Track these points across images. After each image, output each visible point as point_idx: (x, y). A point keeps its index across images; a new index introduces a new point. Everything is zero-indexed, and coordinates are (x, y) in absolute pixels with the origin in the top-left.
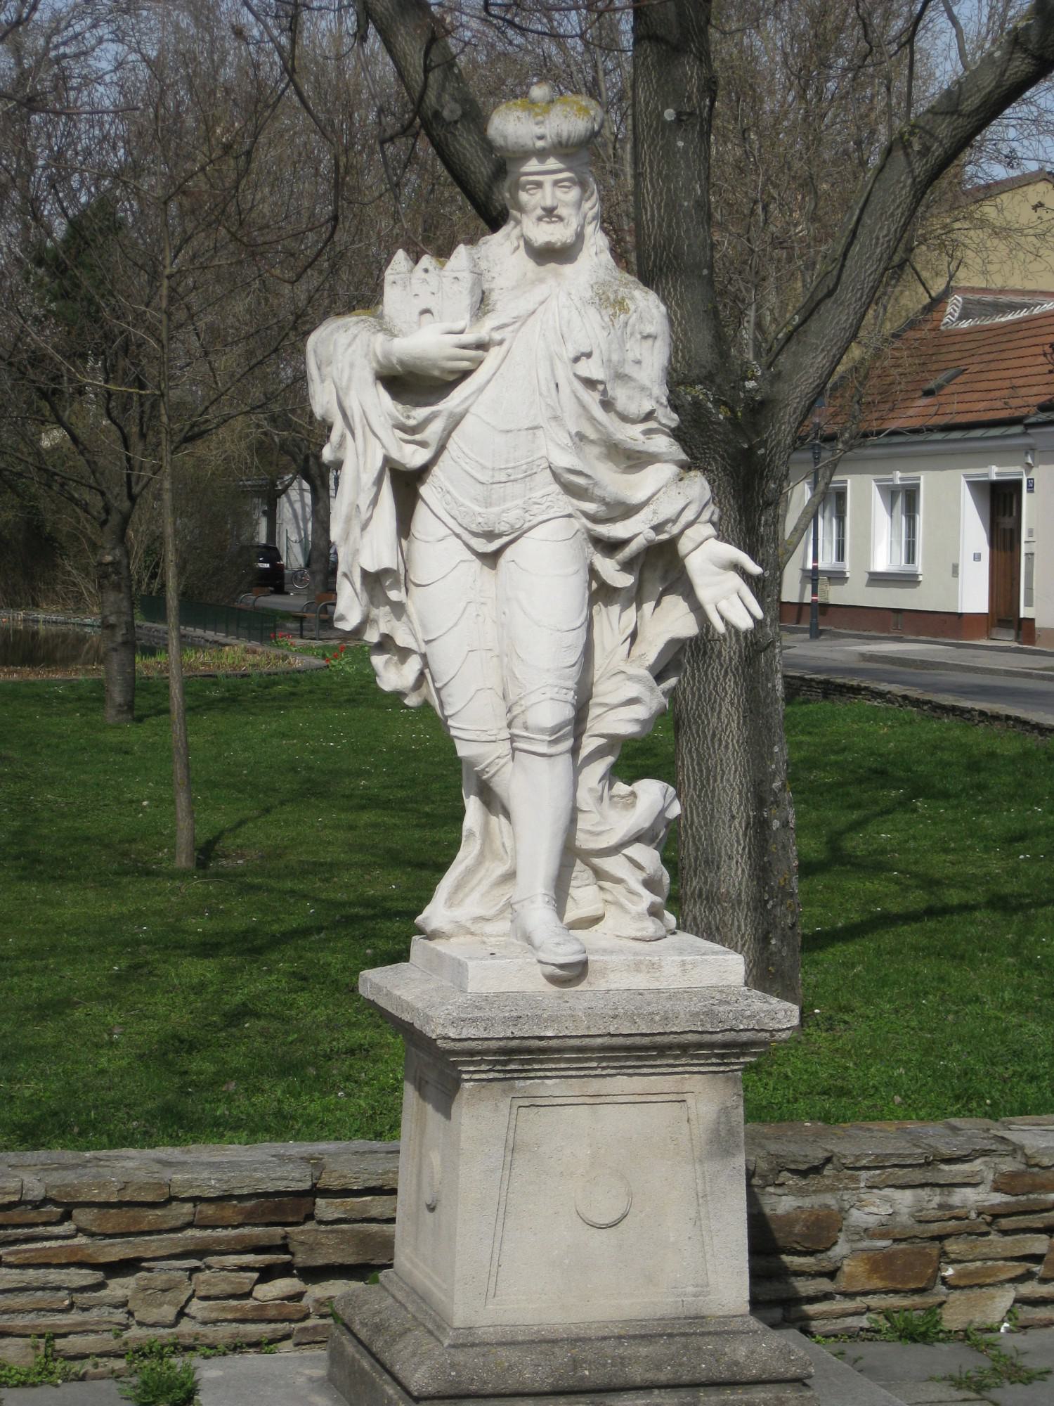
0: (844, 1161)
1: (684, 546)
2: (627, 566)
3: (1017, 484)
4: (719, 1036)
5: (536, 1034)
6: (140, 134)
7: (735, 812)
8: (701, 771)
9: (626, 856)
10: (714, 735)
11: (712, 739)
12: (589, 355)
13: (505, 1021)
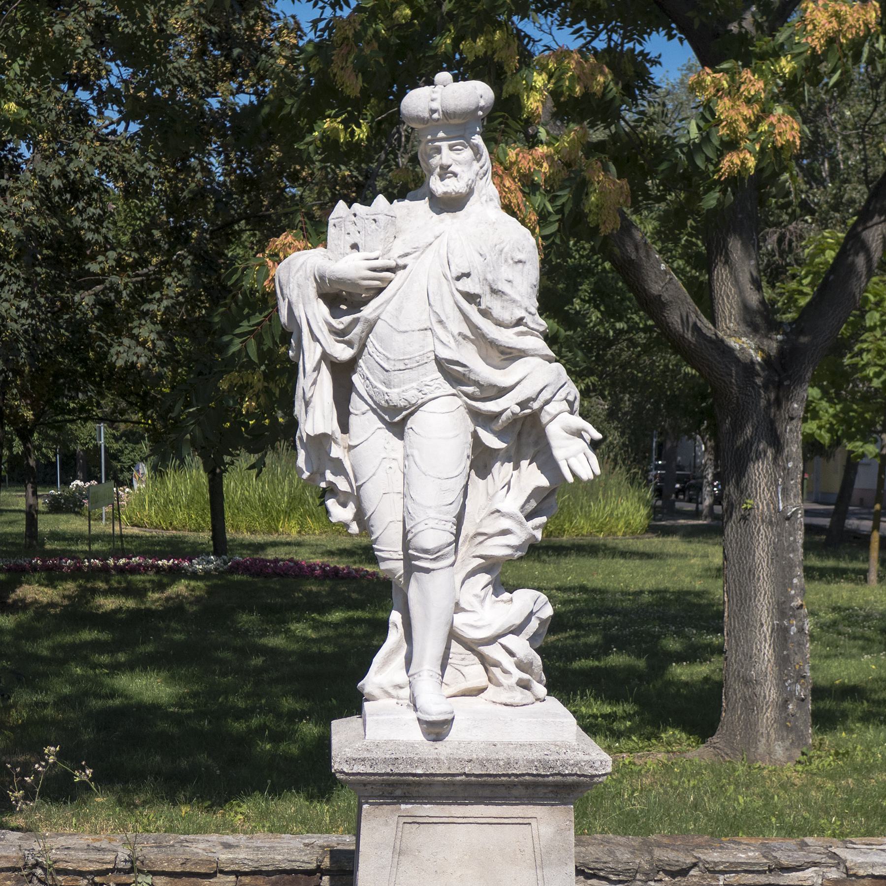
0: (707, 866)
1: (545, 418)
2: (500, 435)
4: (551, 778)
5: (410, 771)
7: (764, 622)
8: (741, 594)
9: (504, 647)
10: (750, 571)
11: (749, 573)
12: (468, 275)
13: (385, 761)
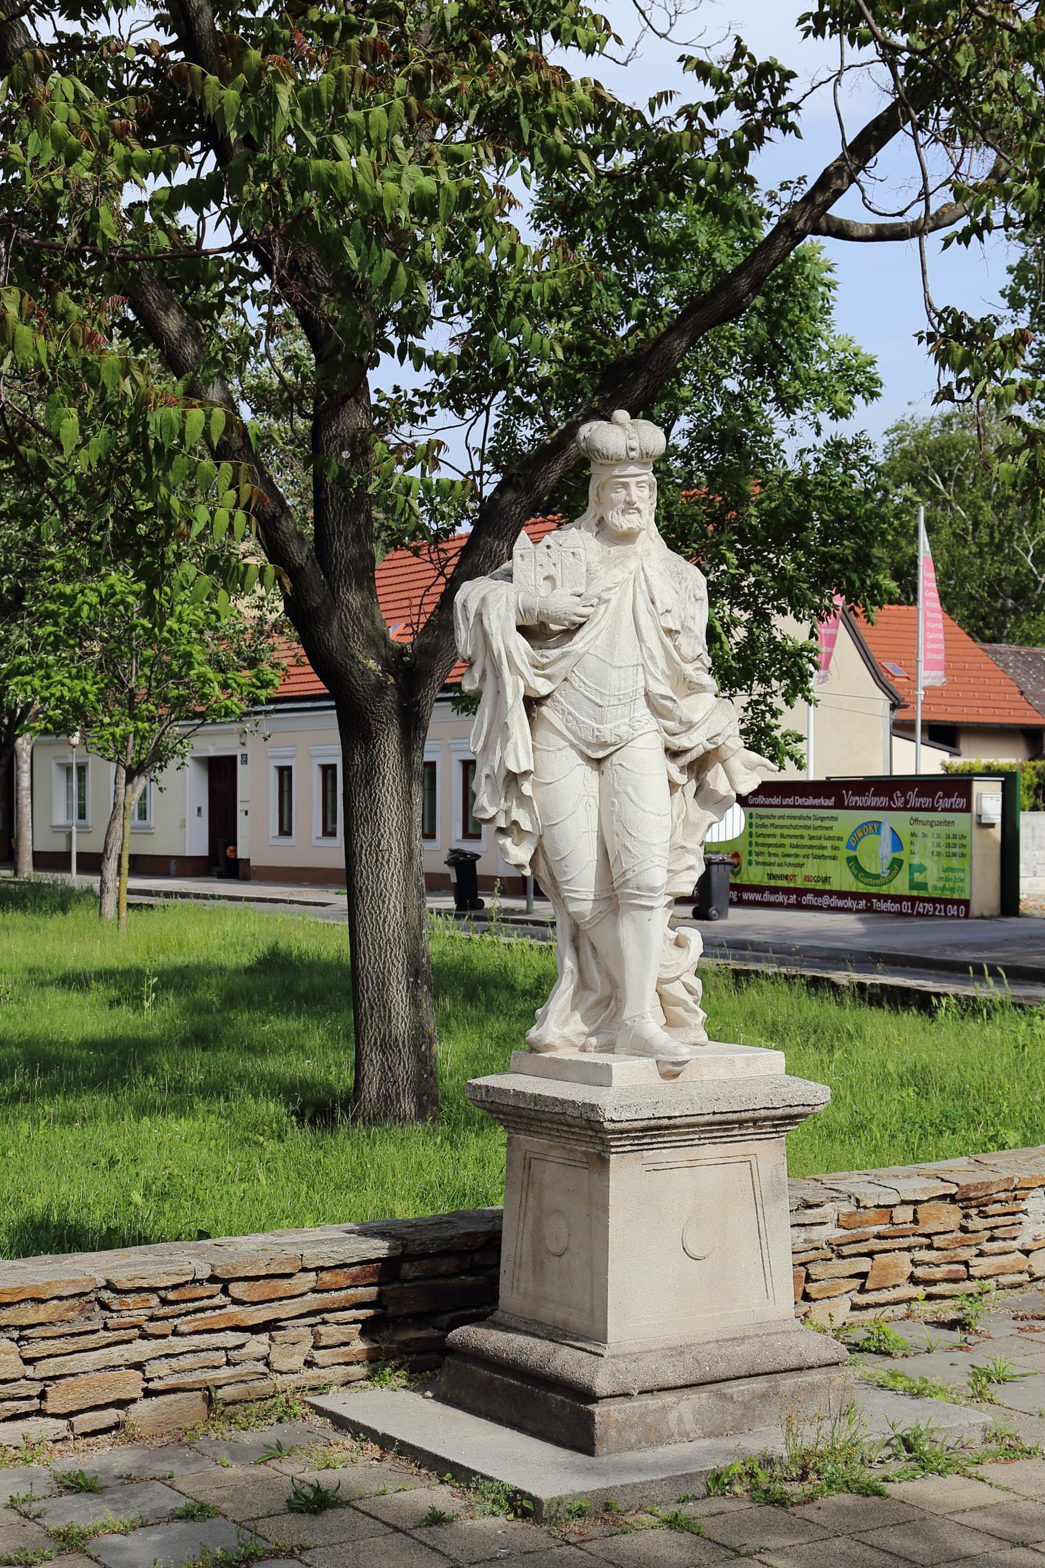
3: (234, 758)
6: (392, 427)
